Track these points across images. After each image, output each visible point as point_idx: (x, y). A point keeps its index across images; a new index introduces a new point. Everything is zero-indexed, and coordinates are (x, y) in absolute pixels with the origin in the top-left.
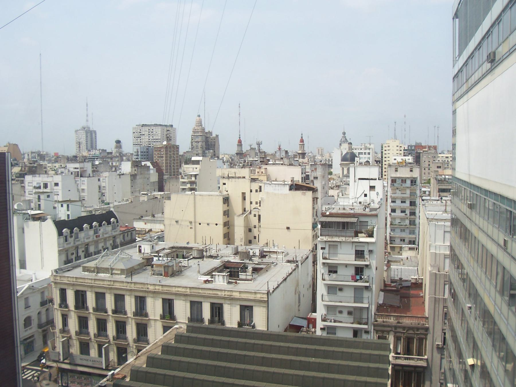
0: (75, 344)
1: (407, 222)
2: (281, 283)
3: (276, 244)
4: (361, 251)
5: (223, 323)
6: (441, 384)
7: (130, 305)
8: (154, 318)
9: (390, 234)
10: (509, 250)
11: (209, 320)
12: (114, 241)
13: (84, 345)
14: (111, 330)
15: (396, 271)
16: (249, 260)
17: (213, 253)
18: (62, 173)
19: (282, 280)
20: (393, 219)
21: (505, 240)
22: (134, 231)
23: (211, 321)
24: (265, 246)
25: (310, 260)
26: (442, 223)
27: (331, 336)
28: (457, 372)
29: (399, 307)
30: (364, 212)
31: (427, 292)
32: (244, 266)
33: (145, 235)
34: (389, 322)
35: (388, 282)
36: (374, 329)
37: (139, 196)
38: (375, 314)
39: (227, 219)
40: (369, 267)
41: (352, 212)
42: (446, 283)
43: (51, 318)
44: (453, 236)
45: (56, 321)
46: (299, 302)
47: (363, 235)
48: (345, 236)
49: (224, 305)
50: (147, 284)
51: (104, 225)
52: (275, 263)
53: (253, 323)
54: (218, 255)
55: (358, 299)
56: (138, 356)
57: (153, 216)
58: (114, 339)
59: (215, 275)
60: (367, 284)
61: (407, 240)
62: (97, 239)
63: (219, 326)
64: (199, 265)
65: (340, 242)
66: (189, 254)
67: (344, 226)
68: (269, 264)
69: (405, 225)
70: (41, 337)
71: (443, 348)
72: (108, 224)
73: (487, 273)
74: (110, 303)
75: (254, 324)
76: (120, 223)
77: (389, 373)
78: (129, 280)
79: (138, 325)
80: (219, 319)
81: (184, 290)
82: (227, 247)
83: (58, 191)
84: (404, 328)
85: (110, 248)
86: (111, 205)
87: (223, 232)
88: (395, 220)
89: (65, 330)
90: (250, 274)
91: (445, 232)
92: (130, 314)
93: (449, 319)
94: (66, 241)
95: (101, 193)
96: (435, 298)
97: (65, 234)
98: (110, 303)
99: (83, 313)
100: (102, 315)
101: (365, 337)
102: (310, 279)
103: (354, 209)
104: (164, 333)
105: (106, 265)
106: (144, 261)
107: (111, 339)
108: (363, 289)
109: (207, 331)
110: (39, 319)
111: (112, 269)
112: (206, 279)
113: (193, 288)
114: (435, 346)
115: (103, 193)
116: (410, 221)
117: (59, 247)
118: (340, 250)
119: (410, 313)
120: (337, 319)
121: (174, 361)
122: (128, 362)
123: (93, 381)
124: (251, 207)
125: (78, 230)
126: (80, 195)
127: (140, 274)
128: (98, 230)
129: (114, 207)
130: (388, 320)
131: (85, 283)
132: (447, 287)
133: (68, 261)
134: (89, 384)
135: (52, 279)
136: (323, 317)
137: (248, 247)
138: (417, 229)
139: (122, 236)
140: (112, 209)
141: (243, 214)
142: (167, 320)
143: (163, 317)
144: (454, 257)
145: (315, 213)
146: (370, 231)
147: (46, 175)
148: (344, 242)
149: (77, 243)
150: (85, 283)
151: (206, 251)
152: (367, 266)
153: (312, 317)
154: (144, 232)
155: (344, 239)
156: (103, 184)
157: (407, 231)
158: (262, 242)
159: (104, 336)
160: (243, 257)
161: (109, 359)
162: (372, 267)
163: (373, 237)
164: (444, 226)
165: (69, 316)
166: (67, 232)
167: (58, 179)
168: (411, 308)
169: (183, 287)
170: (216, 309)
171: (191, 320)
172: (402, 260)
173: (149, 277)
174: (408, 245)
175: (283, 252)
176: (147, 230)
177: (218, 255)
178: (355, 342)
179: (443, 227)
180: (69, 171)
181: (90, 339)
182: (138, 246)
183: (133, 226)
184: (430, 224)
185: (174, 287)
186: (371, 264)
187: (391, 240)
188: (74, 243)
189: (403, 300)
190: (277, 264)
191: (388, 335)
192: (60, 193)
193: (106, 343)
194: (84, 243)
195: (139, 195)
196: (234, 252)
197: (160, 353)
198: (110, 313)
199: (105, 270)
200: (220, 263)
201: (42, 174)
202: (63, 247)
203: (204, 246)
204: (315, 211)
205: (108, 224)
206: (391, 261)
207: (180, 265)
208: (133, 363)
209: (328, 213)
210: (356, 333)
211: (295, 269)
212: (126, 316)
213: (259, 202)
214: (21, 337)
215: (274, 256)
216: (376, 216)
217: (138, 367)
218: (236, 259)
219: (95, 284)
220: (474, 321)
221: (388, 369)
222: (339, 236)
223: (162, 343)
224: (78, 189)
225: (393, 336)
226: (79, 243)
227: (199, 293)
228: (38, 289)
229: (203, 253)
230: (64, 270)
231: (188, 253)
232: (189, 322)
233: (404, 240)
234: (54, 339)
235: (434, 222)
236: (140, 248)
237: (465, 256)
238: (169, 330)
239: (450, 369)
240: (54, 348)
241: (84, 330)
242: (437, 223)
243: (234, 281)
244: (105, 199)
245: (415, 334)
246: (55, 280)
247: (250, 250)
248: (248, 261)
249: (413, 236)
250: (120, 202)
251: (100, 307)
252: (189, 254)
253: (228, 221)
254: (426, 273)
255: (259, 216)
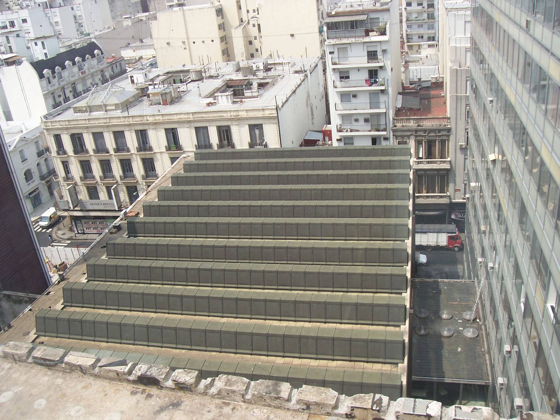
0: (82, 190)
1: (425, 16)
2: (290, 97)
3: (280, 55)
4: (374, 51)
5: (233, 146)
6: (465, 185)
7: (131, 141)
8: (159, 151)
9: (407, 31)
10: (531, 32)
11: (217, 144)
12: (103, 76)
13: (92, 189)
14: (117, 170)
15: (415, 72)
16: (253, 76)
17: (213, 72)
18: (28, 6)
19: (291, 93)
20: (409, 14)
21: (527, 21)
22: (123, 61)
23: (221, 146)
24: (270, 58)
25: (320, 68)
26: (463, 12)
27: (349, 147)
28: (480, 171)
29: (419, 110)
30: (374, 8)
31: (448, 91)
32: (248, 82)
33: (136, 64)
34: (409, 126)
35: (406, 85)
36: (393, 135)
37: (122, 21)
38: (393, 119)
39: (223, 34)
40: (384, 68)
41: (361, 8)
42: (468, 79)
43: (51, 168)
44: (474, 25)
45: (58, 169)
46: (312, 115)
47: (374, 33)
48: (355, 37)
49: (231, 127)
50: (146, 115)
51: (88, 59)
52: (282, 76)
53: (264, 142)
54: (218, 74)
55: (374, 104)
56: (148, 191)
57: (142, 41)
58: (121, 179)
59: (218, 96)
60: (383, 88)
61: (425, 37)
62: (84, 75)
63: (229, 150)
64: (198, 87)
65: (350, 44)
66: (187, 77)
67: (353, 25)
68: (275, 78)
69: (423, 20)
70: (46, 188)
71: (466, 148)
72: (92, 58)
73: (509, 61)
74: (110, 142)
75: (266, 143)
76: (106, 55)
77: (410, 178)
78: (126, 114)
79: (144, 161)
80: (229, 142)
81: (186, 116)
82: (227, 64)
83: (27, 28)
84: (425, 131)
85: (100, 83)
86: (92, 36)
87: (221, 48)
88: (411, 15)
89: (68, 178)
90: (256, 91)
91: (465, 22)
92: (133, 150)
93: (471, 117)
94: (50, 83)
95: (78, 24)
96: (457, 96)
97: (46, 76)
98: (110, 142)
99: (84, 157)
100: (104, 156)
101: (384, 143)
102: (322, 89)
103: (362, 5)
104: (172, 163)
105: (98, 102)
106: (138, 92)
107: (118, 179)
108: (378, 93)
109: (216, 155)
110: (40, 171)
111: (106, 106)
112: (209, 102)
113: (195, 113)
114: (458, 147)
115: (80, 24)
116: (428, 15)
117: (43, 91)
118: (350, 53)
119: (431, 114)
120: (353, 128)
121: (186, 191)
122: (139, 199)
123: (109, 223)
124: (248, 17)
125: (60, 69)
126: (54, 30)
127: (137, 106)
128: (83, 65)
129: (95, 38)
130: (407, 124)
131: (79, 124)
132: (468, 83)
133: (56, 105)
134: (105, 228)
135: (43, 127)
136: (338, 127)
137: (250, 62)
138: (437, 23)
139: (110, 68)
140: (93, 40)
141: (240, 25)
142: (173, 151)
143: (169, 148)
144: (475, 49)
145: (321, 15)
146: (382, 29)
147: (9, 12)
148: (353, 43)
149: (62, 84)
150: (79, 124)
151: (205, 72)
152: (381, 67)
153: (327, 129)
154: (134, 61)
155: (353, 40)
156: (78, 13)
157: (426, 26)
158: (265, 54)
159: (110, 177)
160: (246, 72)
161: (120, 200)
162: (387, 68)
163: (386, 35)
164: (465, 15)
165: (70, 162)
166: (48, 73)
167: (24, 14)
168: (432, 110)
169: (185, 114)
170: (223, 133)
171: (199, 147)
172: (421, 59)
173: (148, 108)
174: (427, 43)
175: (289, 63)
176: (137, 58)
177: (218, 74)
178: (374, 149)
179: (464, 17)
180: (35, 3)
181: (97, 182)
182: (129, 76)
183: (121, 54)
184: (449, 15)
185: (175, 115)
186: (386, 65)
187: (408, 38)
188: (59, 84)
189: (423, 101)
190: (284, 76)
191: (409, 139)
192: (31, 30)
193: (114, 184)
194: (70, 83)
195: (121, 20)
196: (235, 69)
197: (171, 185)
198: (112, 152)
199: (99, 108)
200: (222, 83)
201: (4, 11)
202: (48, 90)
203: (202, 66)
204: (320, 12)
205: (92, 58)
206: (410, 62)
207: (178, 90)
208: (144, 198)
209: (333, 13)
210: (374, 141)
211: (304, 80)
212: (130, 153)
213: (256, 9)
214: (24, 192)
215: (279, 68)
216: (388, 10)
217: (149, 202)
218: (239, 77)
219: (89, 124)
220: (496, 115)
221: (409, 174)
222: (348, 37)
223: (171, 175)
224: (51, 23)
225: (413, 140)
226: (65, 83)
227: (203, 117)
228: (31, 140)
229: (202, 75)
230: (54, 115)
231: (185, 76)
232: (196, 149)
233: (422, 37)
234: (60, 188)
235: (454, 12)
236: (132, 78)
237: (486, 46)
238: (176, 160)
239: (473, 168)
240: (62, 197)
241: (88, 174)
242: (456, 13)
243: (239, 100)
244: (83, 30)
245: (436, 136)
246: (47, 126)
247: (252, 64)
248: (251, 77)
249: (433, 31)
250: (102, 31)
251: (100, 148)
252: (187, 77)
253: (225, 36)
254: (446, 70)
255: (259, 25)
